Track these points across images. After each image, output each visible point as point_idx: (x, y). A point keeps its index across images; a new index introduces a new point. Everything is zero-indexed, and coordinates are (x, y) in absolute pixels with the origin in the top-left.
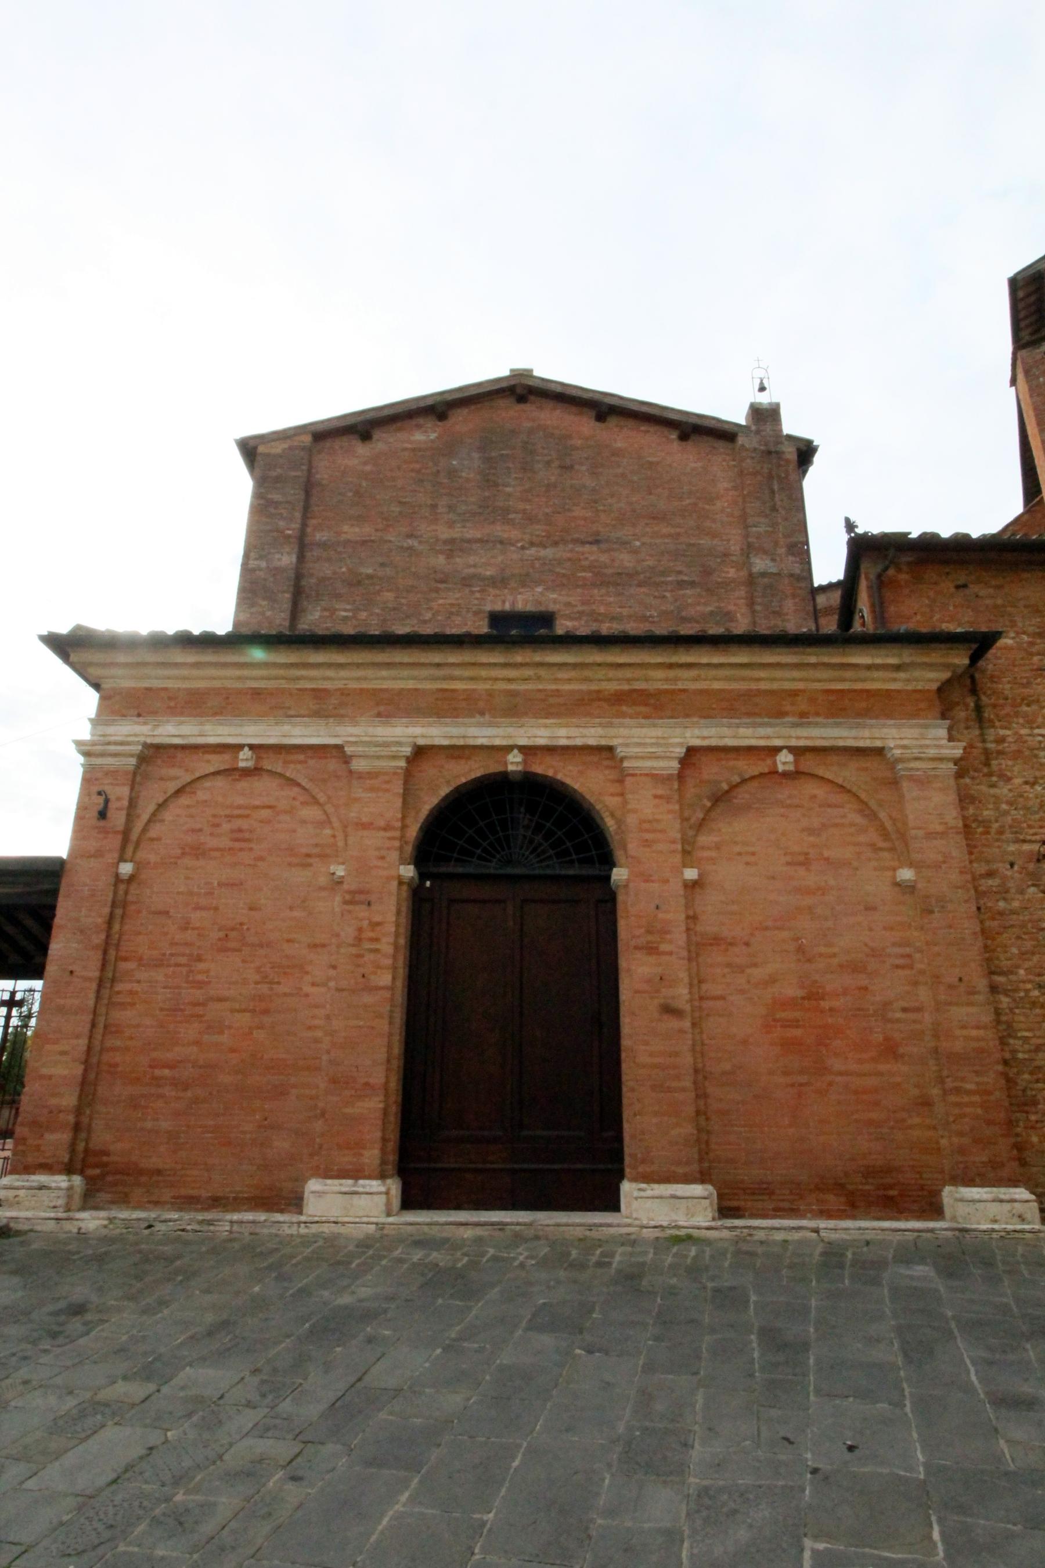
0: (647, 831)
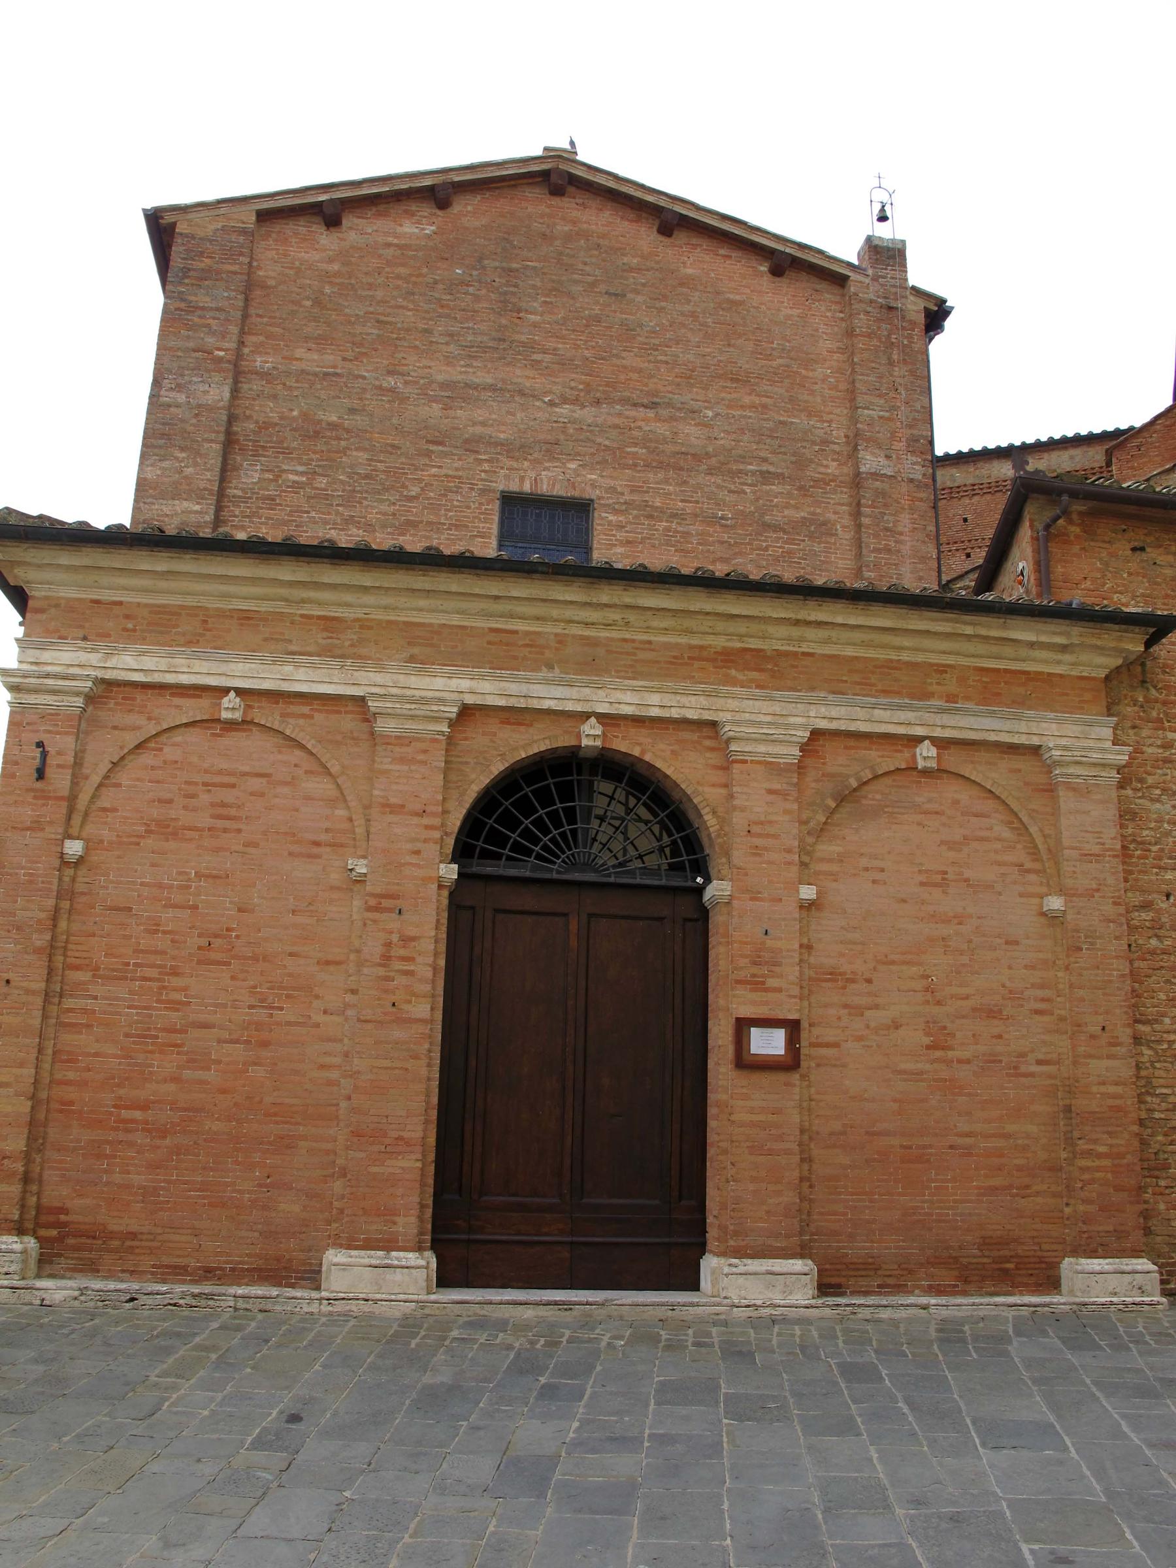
0: (759, 835)
